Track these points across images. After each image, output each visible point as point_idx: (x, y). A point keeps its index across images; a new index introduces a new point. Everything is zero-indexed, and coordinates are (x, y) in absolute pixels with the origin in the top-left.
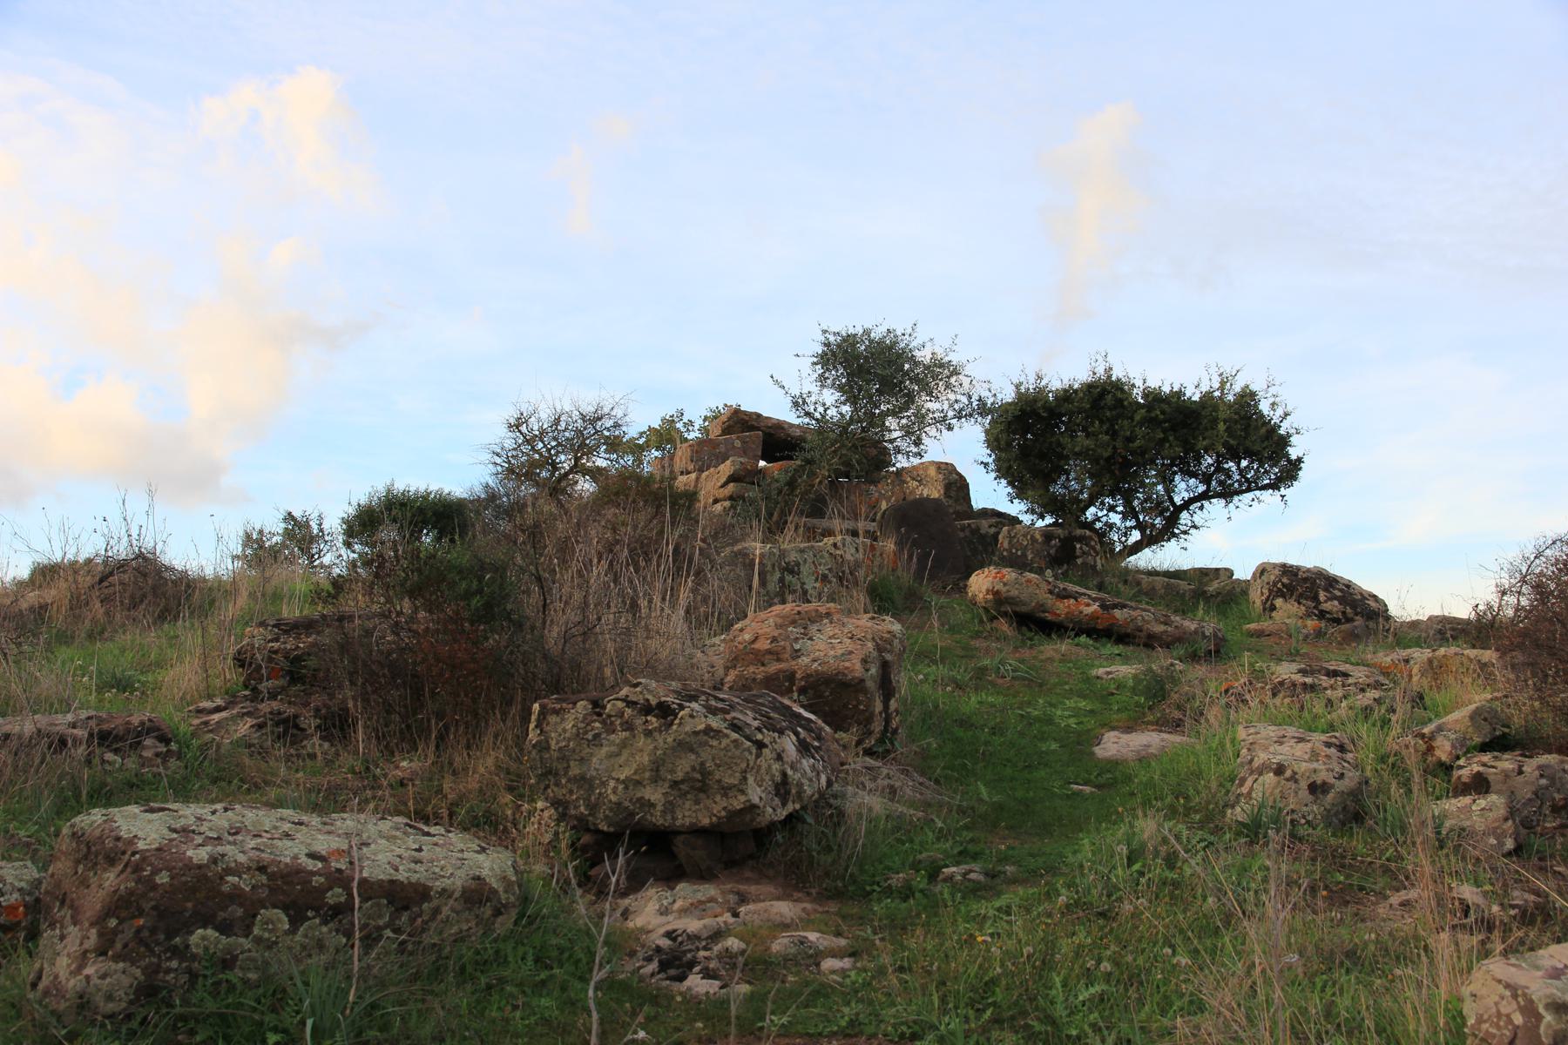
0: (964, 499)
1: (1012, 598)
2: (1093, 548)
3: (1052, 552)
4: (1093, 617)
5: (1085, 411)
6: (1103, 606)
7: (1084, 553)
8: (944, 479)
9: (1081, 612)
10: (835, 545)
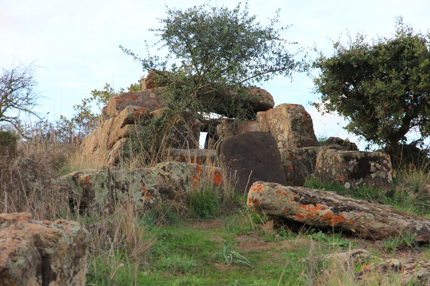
0: (308, 131)
1: (267, 205)
2: (386, 166)
3: (351, 169)
4: (328, 218)
5: (387, 62)
6: (336, 210)
7: (377, 169)
8: (291, 117)
9: (318, 214)
10: (164, 168)
